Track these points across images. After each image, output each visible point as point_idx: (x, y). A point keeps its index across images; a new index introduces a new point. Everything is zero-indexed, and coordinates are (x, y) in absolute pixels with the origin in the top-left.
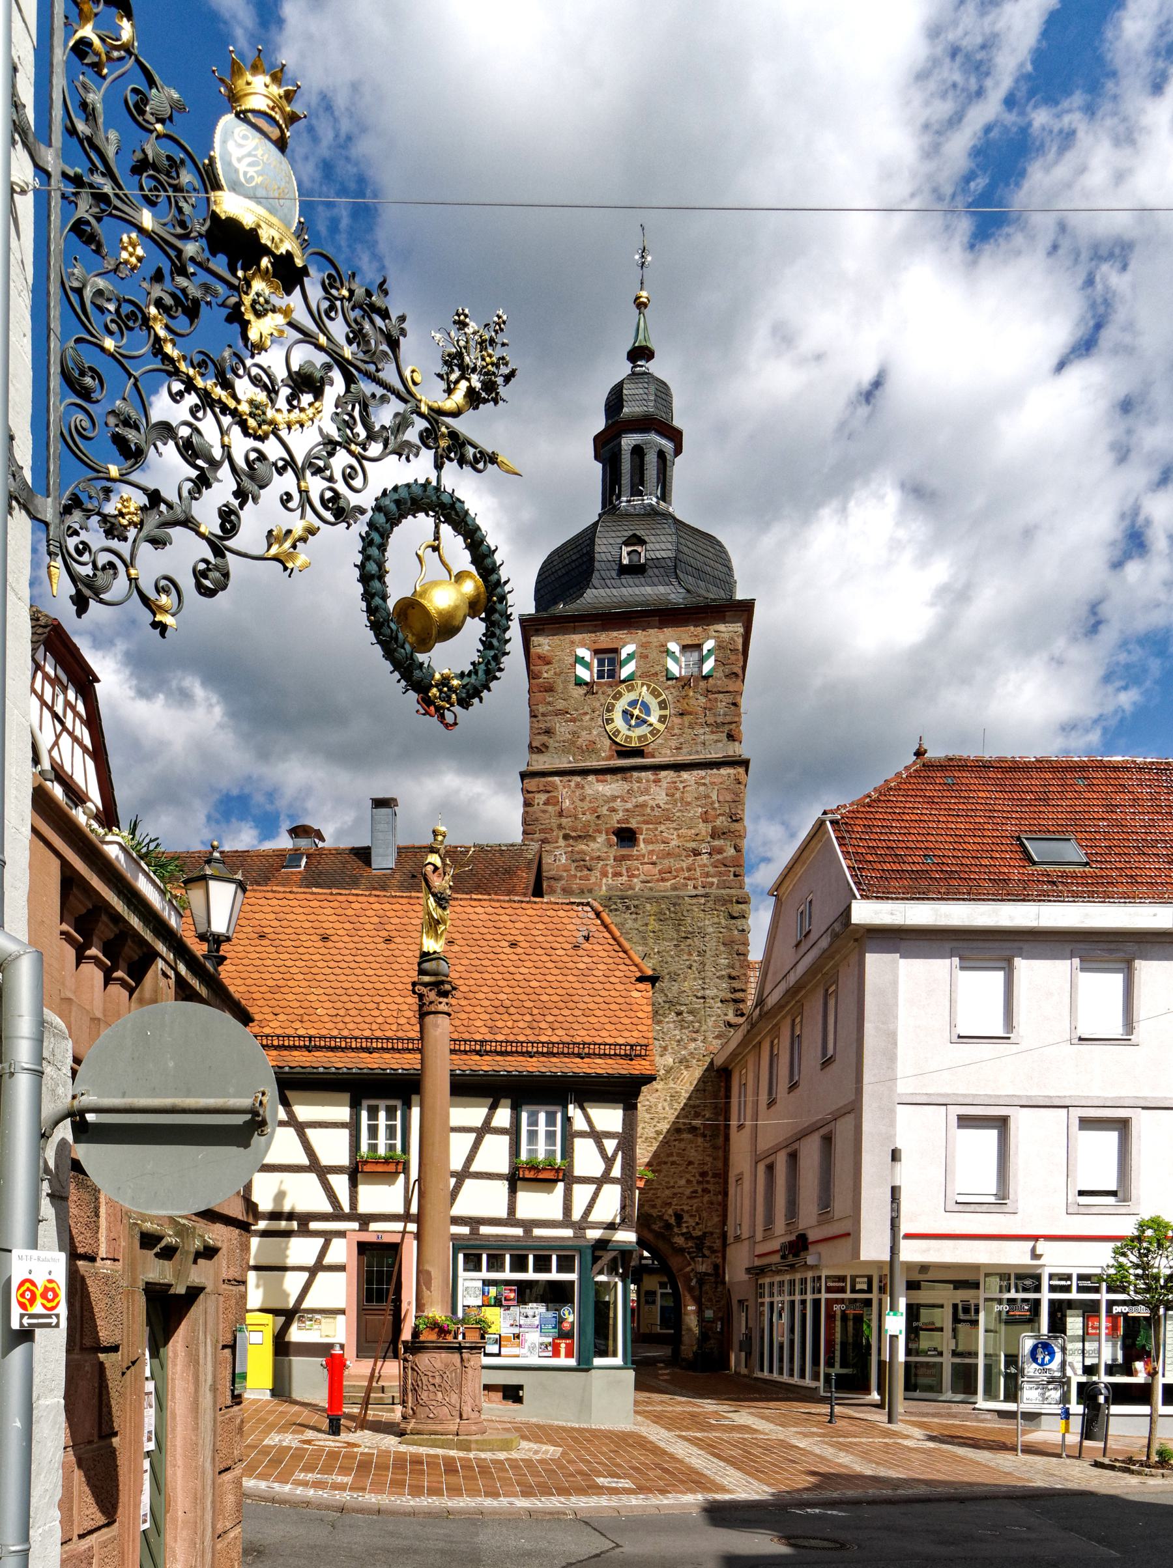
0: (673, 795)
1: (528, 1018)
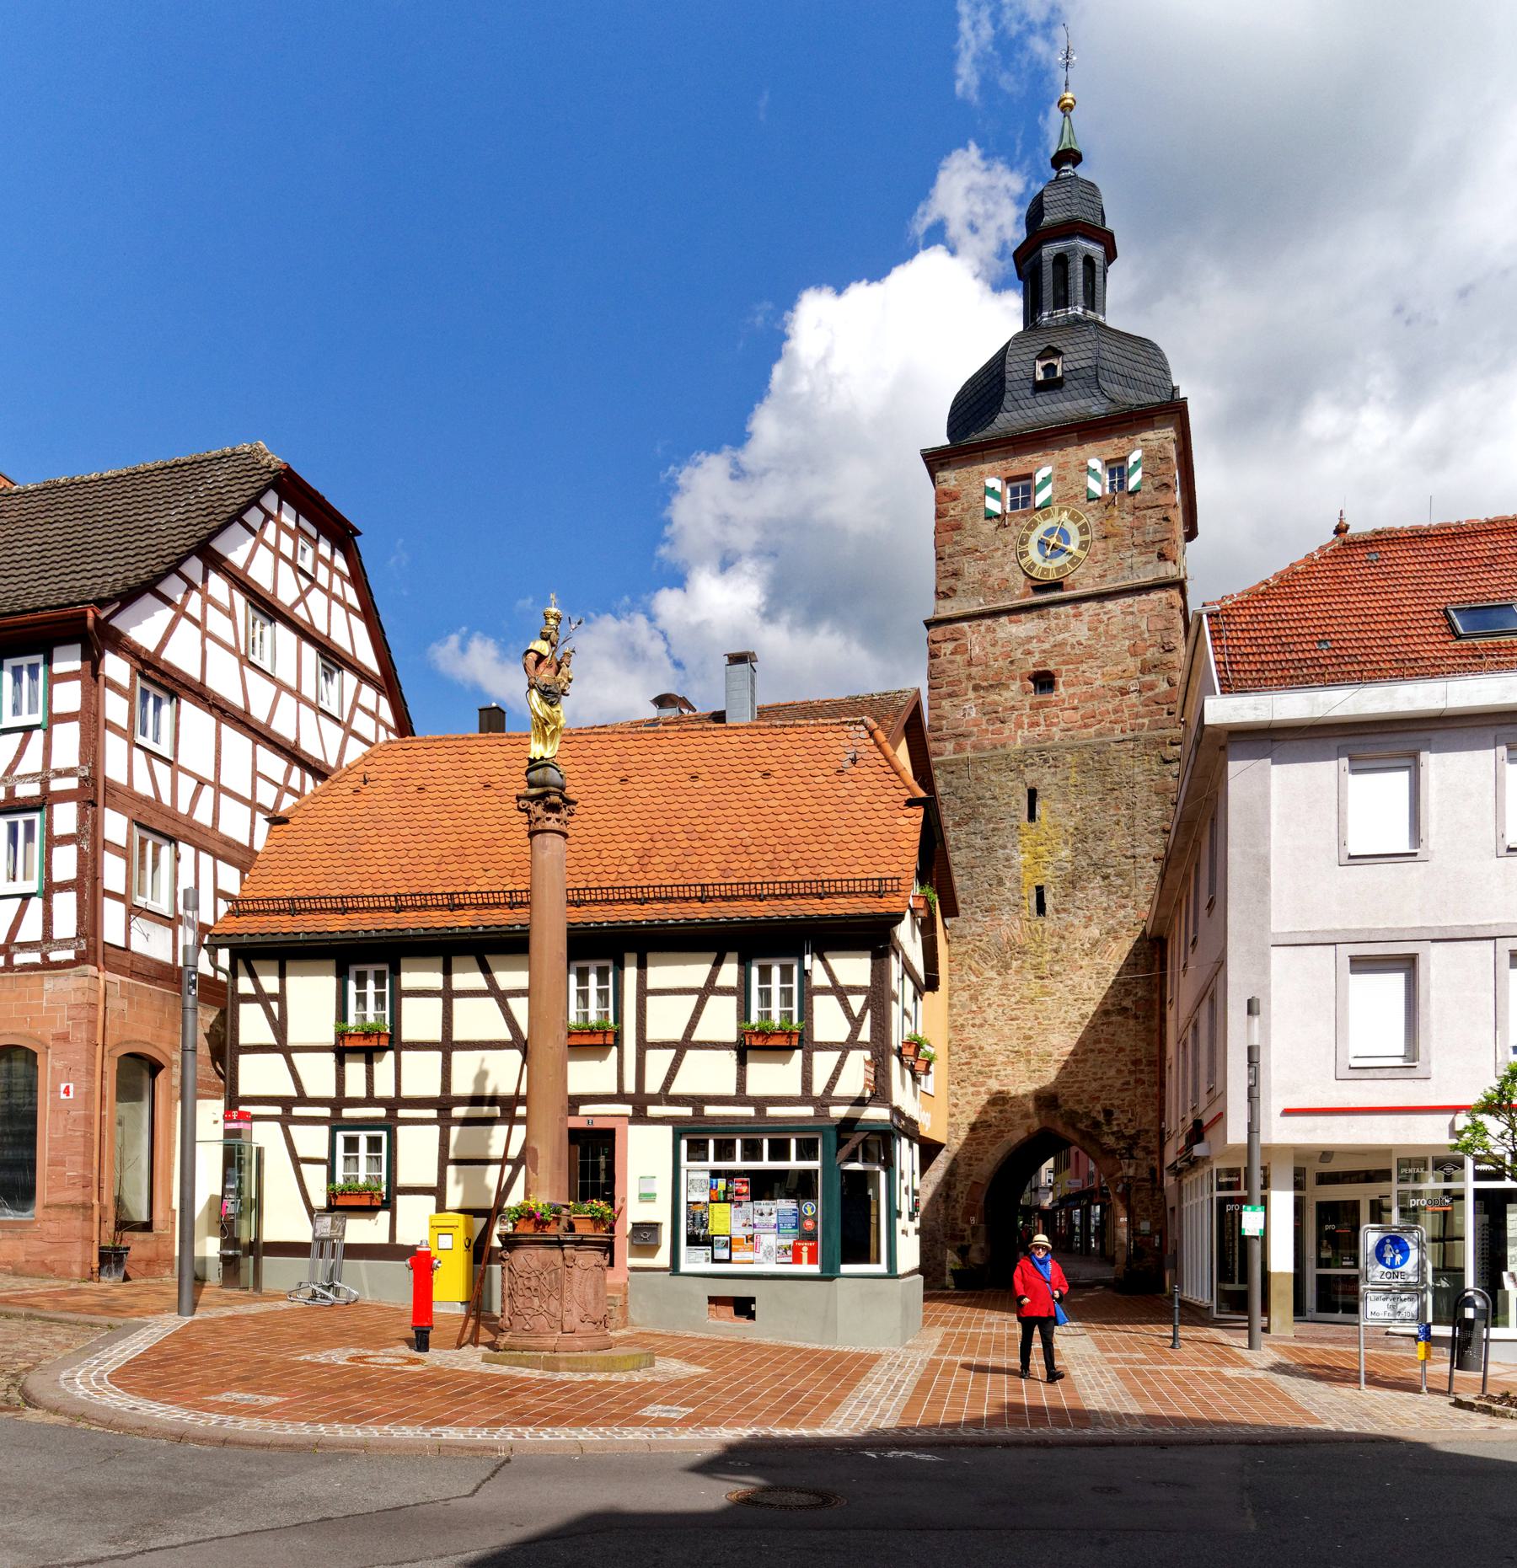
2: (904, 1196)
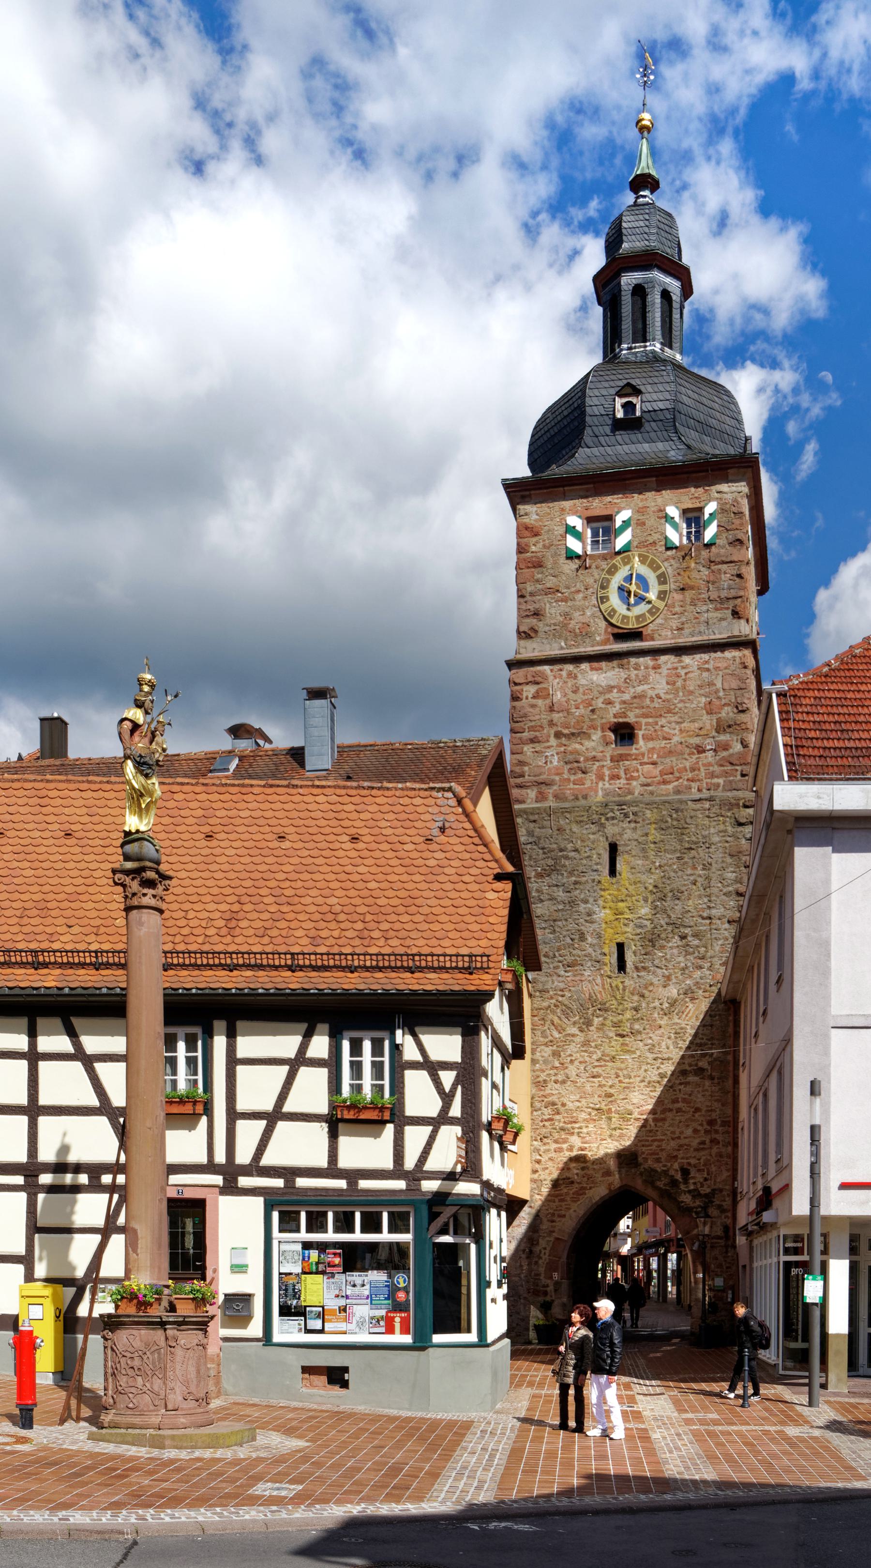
0: (674, 683)
1: (359, 926)
2: (493, 1264)
